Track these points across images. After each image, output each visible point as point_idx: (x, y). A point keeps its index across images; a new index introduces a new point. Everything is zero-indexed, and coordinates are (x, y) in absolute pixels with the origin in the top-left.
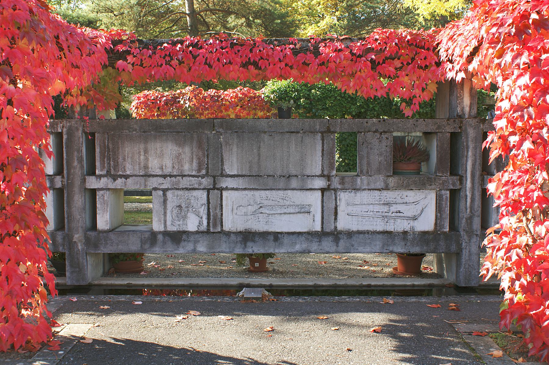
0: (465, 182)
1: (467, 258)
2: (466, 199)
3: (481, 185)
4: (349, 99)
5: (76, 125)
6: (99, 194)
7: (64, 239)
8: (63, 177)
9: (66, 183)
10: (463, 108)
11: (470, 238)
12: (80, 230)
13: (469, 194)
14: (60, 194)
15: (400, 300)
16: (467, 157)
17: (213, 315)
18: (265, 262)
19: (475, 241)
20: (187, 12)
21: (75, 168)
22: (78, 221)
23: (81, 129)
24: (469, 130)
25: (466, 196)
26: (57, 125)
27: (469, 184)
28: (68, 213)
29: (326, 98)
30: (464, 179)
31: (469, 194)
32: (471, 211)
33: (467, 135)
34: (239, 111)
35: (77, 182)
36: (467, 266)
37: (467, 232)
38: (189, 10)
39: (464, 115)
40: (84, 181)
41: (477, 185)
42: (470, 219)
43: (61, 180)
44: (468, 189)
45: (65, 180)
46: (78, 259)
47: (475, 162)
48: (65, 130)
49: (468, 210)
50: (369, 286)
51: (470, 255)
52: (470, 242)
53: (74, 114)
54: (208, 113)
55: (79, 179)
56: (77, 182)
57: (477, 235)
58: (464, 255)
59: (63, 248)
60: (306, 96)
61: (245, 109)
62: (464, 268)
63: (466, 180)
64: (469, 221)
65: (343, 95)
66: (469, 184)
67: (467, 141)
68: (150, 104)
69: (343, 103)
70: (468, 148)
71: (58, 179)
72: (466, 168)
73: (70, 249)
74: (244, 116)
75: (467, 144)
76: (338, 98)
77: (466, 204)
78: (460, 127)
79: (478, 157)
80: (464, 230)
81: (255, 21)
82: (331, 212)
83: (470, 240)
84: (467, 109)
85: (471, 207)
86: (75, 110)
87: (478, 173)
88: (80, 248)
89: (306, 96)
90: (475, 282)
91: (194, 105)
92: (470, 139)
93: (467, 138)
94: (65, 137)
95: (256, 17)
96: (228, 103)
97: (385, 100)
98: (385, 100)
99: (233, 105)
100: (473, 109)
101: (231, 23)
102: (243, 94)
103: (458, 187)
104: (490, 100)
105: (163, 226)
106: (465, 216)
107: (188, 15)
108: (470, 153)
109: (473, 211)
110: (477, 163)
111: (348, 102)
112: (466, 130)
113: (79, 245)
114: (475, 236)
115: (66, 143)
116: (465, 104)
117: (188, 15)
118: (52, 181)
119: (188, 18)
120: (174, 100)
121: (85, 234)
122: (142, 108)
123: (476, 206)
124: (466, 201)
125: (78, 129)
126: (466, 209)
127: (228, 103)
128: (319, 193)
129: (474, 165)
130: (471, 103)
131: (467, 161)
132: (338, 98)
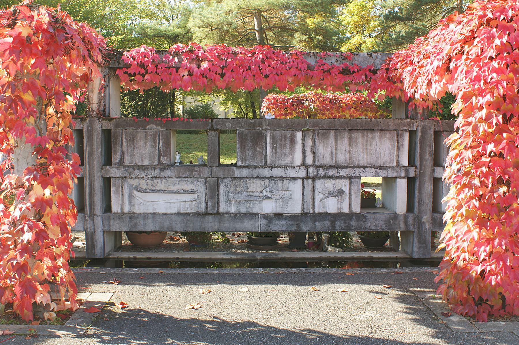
5: (429, 125)
6: (112, 180)
7: (414, 219)
8: (416, 168)
9: (418, 173)
12: (428, 212)
14: (411, 182)
17: (249, 284)
18: (87, 239)
20: (256, 28)
21: (426, 160)
22: (427, 205)
23: (433, 128)
26: (413, 124)
28: (419, 198)
34: (353, 112)
35: (428, 172)
38: (258, 27)
40: (433, 171)
43: (414, 170)
45: (418, 171)
46: (425, 236)
48: (419, 128)
53: (417, 115)
54: (329, 114)
55: (430, 169)
56: (428, 172)
59: (414, 228)
61: (358, 110)
68: (281, 106)
71: (412, 169)
73: (419, 228)
74: (356, 116)
81: (317, 37)
86: (418, 111)
88: (427, 227)
91: (318, 106)
94: (419, 134)
95: (316, 34)
96: (344, 105)
99: (349, 107)
102: (357, 98)
105: (120, 207)
107: (258, 31)
113: (427, 224)
115: (420, 140)
118: (407, 172)
119: (257, 34)
120: (299, 102)
121: (432, 215)
122: (273, 109)
125: (430, 128)
127: (344, 105)
128: (300, 182)
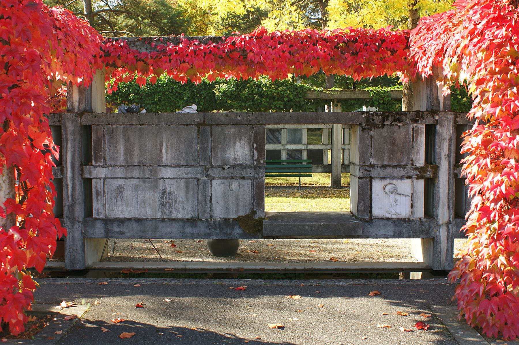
0: (65, 172)
1: (71, 243)
2: (68, 187)
3: (81, 174)
4: (177, 94)
10: (73, 103)
11: (73, 224)
13: (70, 183)
15: (352, 283)
16: (66, 148)
19: (78, 227)
24: (67, 123)
25: (67, 185)
27: (69, 174)
29: (155, 93)
30: (65, 169)
31: (70, 183)
32: (72, 199)
33: (66, 128)
36: (71, 251)
37: (69, 219)
38: (86, 11)
39: (74, 109)
41: (77, 175)
42: (72, 207)
44: (68, 178)
47: (75, 154)
49: (70, 198)
50: (144, 269)
51: (74, 240)
52: (73, 228)
57: (79, 222)
58: (68, 240)
60: (136, 91)
62: (69, 252)
63: (67, 170)
64: (71, 208)
65: (170, 91)
66: (69, 174)
67: (66, 134)
69: (171, 97)
70: (67, 140)
72: (66, 158)
75: (66, 137)
76: (167, 93)
77: (68, 192)
78: (59, 121)
79: (77, 149)
80: (67, 217)
82: (365, 199)
83: (73, 226)
84: (76, 104)
85: (73, 196)
87: (77, 164)
89: (136, 91)
90: (79, 265)
92: (69, 132)
93: (66, 131)
97: (209, 95)
98: (209, 95)
100: (82, 104)
101: (122, 23)
103: (60, 177)
104: (312, 94)
106: (67, 204)
108: (69, 145)
109: (74, 200)
110: (77, 154)
111: (177, 97)
112: (65, 123)
114: (77, 223)
116: (74, 99)
117: (86, 15)
123: (77, 195)
124: (68, 190)
126: (68, 197)
129: (73, 156)
130: (80, 99)
131: (66, 152)
132: (167, 93)
